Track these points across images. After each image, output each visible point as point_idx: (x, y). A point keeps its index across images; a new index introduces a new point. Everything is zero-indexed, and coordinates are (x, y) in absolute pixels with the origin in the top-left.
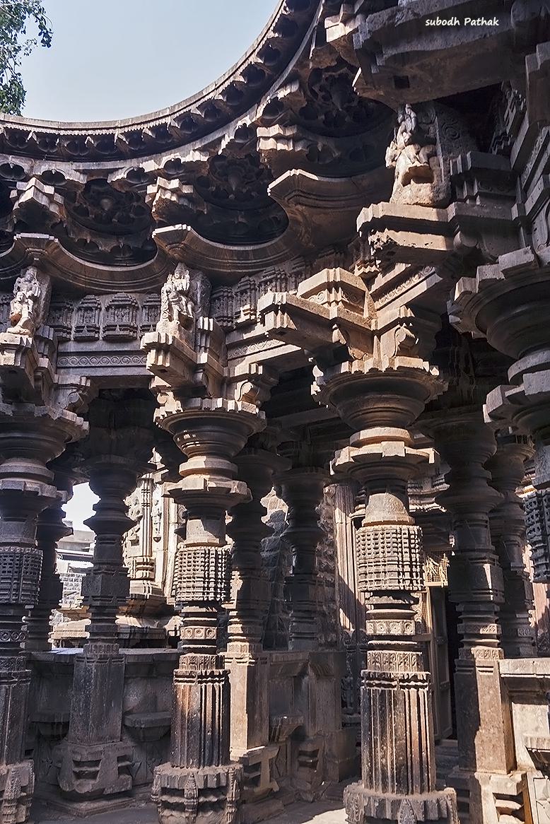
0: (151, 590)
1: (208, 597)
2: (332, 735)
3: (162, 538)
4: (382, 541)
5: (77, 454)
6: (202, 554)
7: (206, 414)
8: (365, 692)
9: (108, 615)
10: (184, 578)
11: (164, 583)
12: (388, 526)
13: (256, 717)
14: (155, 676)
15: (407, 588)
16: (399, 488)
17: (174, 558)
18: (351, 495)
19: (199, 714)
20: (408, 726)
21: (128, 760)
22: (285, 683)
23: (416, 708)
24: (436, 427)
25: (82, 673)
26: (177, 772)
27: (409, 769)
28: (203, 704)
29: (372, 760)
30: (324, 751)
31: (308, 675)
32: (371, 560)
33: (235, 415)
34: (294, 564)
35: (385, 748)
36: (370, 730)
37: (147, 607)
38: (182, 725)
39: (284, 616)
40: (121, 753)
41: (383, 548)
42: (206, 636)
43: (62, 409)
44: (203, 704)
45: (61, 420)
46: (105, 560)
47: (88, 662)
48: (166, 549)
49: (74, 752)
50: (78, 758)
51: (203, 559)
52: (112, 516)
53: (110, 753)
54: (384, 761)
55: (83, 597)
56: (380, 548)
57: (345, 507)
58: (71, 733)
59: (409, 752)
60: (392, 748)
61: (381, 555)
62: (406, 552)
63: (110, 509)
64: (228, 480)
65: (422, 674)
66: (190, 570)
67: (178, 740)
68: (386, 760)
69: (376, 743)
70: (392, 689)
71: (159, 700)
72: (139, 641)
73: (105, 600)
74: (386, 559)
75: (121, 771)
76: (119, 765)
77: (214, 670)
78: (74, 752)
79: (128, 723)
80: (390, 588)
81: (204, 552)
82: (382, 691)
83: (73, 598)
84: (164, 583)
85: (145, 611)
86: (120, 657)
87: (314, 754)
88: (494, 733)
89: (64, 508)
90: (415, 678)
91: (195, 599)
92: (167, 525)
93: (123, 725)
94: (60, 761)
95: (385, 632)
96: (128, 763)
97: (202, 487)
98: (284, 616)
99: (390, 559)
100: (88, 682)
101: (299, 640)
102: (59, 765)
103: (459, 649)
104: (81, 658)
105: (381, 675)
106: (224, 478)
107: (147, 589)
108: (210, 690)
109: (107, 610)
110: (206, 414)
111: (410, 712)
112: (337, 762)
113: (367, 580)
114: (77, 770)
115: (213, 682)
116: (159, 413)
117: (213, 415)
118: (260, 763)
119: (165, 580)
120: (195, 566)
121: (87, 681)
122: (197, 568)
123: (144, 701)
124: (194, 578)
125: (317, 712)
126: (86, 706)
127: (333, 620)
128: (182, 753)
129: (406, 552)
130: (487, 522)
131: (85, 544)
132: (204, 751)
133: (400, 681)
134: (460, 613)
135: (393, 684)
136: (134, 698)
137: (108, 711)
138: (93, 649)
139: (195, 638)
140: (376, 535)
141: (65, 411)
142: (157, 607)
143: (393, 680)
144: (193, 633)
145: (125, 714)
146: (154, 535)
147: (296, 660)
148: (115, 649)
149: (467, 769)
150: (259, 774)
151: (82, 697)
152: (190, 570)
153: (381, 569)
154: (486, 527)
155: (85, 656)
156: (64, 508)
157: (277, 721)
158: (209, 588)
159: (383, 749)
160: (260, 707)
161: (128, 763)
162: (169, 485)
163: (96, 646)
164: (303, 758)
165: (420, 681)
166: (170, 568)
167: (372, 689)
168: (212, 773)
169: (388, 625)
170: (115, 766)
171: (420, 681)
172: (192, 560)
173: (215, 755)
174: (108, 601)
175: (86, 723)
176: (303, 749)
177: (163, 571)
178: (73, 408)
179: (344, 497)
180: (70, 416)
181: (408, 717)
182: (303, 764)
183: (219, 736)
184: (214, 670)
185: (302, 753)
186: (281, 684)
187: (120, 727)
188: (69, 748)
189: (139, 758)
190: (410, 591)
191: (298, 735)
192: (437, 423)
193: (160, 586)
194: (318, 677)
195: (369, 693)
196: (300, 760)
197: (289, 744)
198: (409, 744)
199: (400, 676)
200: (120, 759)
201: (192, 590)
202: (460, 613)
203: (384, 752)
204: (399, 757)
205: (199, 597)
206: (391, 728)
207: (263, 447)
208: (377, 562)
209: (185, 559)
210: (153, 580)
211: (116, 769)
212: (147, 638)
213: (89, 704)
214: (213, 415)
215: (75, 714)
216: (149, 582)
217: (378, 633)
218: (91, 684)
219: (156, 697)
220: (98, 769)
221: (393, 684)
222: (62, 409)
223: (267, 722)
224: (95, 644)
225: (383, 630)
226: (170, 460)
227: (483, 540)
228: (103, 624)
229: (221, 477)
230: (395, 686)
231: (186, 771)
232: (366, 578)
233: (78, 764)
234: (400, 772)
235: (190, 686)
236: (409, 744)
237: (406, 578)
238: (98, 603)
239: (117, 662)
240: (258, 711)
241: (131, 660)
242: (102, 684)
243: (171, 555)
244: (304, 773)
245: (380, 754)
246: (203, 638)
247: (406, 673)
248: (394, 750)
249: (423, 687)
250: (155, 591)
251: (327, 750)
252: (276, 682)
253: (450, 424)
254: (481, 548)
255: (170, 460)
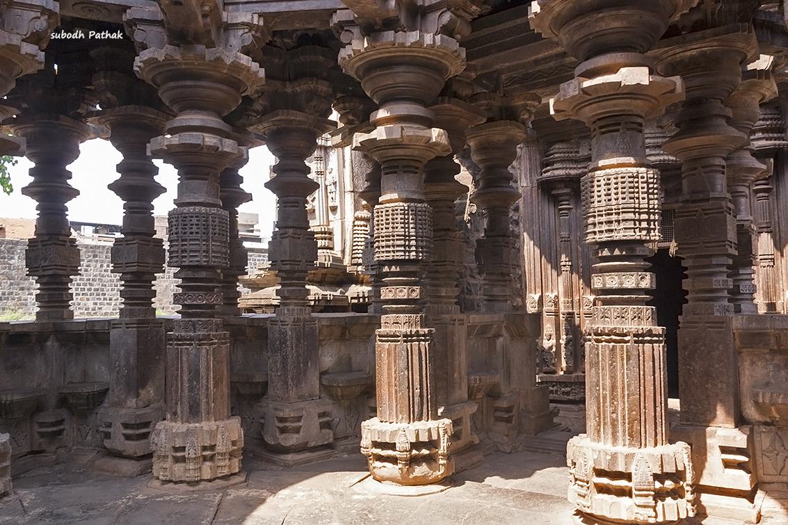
0: (331, 259)
1: (409, 256)
2: (527, 392)
3: (339, 208)
4: (615, 191)
5: (250, 113)
6: (401, 210)
7: (400, 51)
8: (592, 347)
9: (297, 279)
10: (383, 237)
11: (343, 252)
12: (623, 169)
13: (455, 375)
14: (348, 338)
15: (644, 238)
16: (635, 126)
17: (352, 227)
18: (538, 157)
19: (406, 372)
20: (642, 381)
21: (327, 416)
22: (479, 344)
23: (651, 363)
24: (670, 58)
25: (277, 336)
26: (387, 427)
27: (643, 424)
28: (410, 363)
29: (600, 415)
30: (519, 407)
31: (502, 336)
32: (601, 209)
33: (433, 51)
34: (485, 226)
35: (615, 403)
36: (598, 385)
37: (329, 276)
38: (389, 383)
39: (472, 281)
40: (321, 410)
41: (617, 194)
42: (409, 295)
43: (234, 53)
44: (410, 363)
45: (236, 66)
46: (290, 223)
47: (282, 325)
48: (343, 218)
49: (276, 409)
50: (281, 414)
51: (403, 216)
52: (293, 177)
53: (310, 409)
54: (614, 416)
55: (270, 262)
56: (613, 194)
57: (530, 169)
58: (271, 391)
59: (642, 407)
60: (624, 403)
61: (614, 202)
62: (643, 198)
63: (293, 170)
64: (426, 129)
65: (659, 330)
66: (388, 228)
67: (386, 397)
68: (617, 414)
69: (604, 397)
70: (625, 345)
71: (353, 360)
72: (323, 308)
73: (294, 264)
74: (620, 207)
75: (324, 426)
76: (321, 420)
77: (419, 329)
78: (276, 409)
79: (325, 382)
80: (624, 238)
81: (403, 208)
82: (613, 346)
83: (257, 267)
84: (343, 252)
85: (326, 280)
86: (313, 319)
87: (509, 410)
88: (722, 388)
89: (241, 172)
90: (650, 333)
91: (396, 258)
92: (342, 193)
93: (321, 384)
94: (263, 418)
95: (617, 285)
96: (328, 419)
97: (399, 136)
98: (472, 281)
99: (626, 206)
100: (284, 343)
101: (491, 303)
102: (262, 421)
103: (683, 305)
104: (274, 321)
105: (611, 331)
106: (422, 127)
107: (327, 258)
108: (416, 349)
109: (296, 275)
110: (400, 51)
111: (644, 368)
112: (532, 417)
113: (596, 230)
114: (281, 425)
115: (419, 341)
116: (344, 53)
117: (409, 52)
118: (122, 424)
119: (344, 249)
120: (393, 223)
121: (283, 342)
122: (396, 225)
123: (339, 362)
124: (394, 236)
125: (512, 370)
126: (284, 367)
127: (519, 285)
128: (391, 409)
129: (643, 198)
130: (723, 167)
131: (249, 225)
132: (413, 407)
133: (635, 335)
134: (686, 269)
135: (626, 338)
136: (328, 358)
137: (305, 371)
138: (286, 312)
139: (398, 297)
140: (609, 179)
141: (239, 54)
142: (338, 275)
143: (625, 335)
144: (395, 292)
145: (322, 374)
146: (331, 204)
147: (492, 321)
148: (307, 312)
149: (689, 423)
150: (461, 428)
151: (279, 358)
152: (388, 228)
153: (614, 217)
154: (723, 173)
155: (278, 319)
156: (241, 172)
157: (475, 380)
158: (410, 246)
159: (613, 404)
160: (459, 366)
161: (328, 419)
162: (360, 135)
163: (288, 310)
164: (499, 414)
165: (656, 336)
166: (348, 237)
167: (600, 344)
168: (422, 427)
169: (619, 278)
170: (317, 422)
171: (656, 336)
172: (390, 217)
173: (425, 410)
174: (297, 265)
175: (286, 383)
176: (499, 406)
177: (342, 240)
178: (246, 51)
179: (530, 159)
180: (245, 60)
181: (642, 373)
182: (498, 419)
183: (427, 393)
184: (419, 329)
185: (497, 409)
186: (476, 345)
187: (318, 386)
188: (271, 406)
189: (337, 414)
190: (646, 241)
191: (493, 394)
192: (672, 52)
193: (339, 255)
194: (513, 338)
195: (597, 349)
196: (496, 415)
197: (485, 400)
198: (642, 399)
199: (634, 331)
200: (321, 415)
201: (391, 249)
202: (686, 269)
203: (615, 407)
204: (632, 411)
205: (400, 256)
206: (623, 383)
207: (455, 95)
208: (608, 210)
209: (382, 216)
210: (332, 249)
211: (317, 424)
212: (331, 304)
213: (287, 365)
214: (409, 52)
215: (273, 374)
216: (328, 251)
217: (608, 286)
218: (287, 346)
219: (350, 358)
220: (300, 424)
221: (626, 338)
222: (234, 53)
223: (466, 381)
224: (287, 307)
225: (614, 283)
226: (351, 117)
227: (719, 187)
228: (294, 288)
229: (417, 126)
230: (628, 342)
231: (395, 426)
232: (595, 227)
233: (282, 420)
234: (633, 426)
235: (396, 345)
236: (642, 399)
237: (642, 226)
238: (288, 267)
239: (310, 324)
240: (457, 369)
241: (324, 323)
242: (297, 346)
243: (349, 225)
244: (501, 427)
245: (609, 409)
246: (405, 297)
247: (641, 327)
248: (626, 405)
249: (661, 342)
250: (335, 259)
251: (522, 406)
252: (472, 343)
253: (688, 53)
254: (716, 196)
255: (351, 117)
